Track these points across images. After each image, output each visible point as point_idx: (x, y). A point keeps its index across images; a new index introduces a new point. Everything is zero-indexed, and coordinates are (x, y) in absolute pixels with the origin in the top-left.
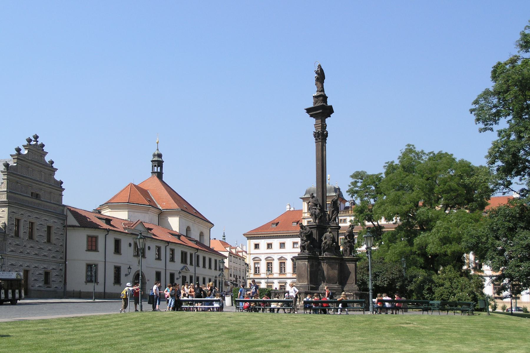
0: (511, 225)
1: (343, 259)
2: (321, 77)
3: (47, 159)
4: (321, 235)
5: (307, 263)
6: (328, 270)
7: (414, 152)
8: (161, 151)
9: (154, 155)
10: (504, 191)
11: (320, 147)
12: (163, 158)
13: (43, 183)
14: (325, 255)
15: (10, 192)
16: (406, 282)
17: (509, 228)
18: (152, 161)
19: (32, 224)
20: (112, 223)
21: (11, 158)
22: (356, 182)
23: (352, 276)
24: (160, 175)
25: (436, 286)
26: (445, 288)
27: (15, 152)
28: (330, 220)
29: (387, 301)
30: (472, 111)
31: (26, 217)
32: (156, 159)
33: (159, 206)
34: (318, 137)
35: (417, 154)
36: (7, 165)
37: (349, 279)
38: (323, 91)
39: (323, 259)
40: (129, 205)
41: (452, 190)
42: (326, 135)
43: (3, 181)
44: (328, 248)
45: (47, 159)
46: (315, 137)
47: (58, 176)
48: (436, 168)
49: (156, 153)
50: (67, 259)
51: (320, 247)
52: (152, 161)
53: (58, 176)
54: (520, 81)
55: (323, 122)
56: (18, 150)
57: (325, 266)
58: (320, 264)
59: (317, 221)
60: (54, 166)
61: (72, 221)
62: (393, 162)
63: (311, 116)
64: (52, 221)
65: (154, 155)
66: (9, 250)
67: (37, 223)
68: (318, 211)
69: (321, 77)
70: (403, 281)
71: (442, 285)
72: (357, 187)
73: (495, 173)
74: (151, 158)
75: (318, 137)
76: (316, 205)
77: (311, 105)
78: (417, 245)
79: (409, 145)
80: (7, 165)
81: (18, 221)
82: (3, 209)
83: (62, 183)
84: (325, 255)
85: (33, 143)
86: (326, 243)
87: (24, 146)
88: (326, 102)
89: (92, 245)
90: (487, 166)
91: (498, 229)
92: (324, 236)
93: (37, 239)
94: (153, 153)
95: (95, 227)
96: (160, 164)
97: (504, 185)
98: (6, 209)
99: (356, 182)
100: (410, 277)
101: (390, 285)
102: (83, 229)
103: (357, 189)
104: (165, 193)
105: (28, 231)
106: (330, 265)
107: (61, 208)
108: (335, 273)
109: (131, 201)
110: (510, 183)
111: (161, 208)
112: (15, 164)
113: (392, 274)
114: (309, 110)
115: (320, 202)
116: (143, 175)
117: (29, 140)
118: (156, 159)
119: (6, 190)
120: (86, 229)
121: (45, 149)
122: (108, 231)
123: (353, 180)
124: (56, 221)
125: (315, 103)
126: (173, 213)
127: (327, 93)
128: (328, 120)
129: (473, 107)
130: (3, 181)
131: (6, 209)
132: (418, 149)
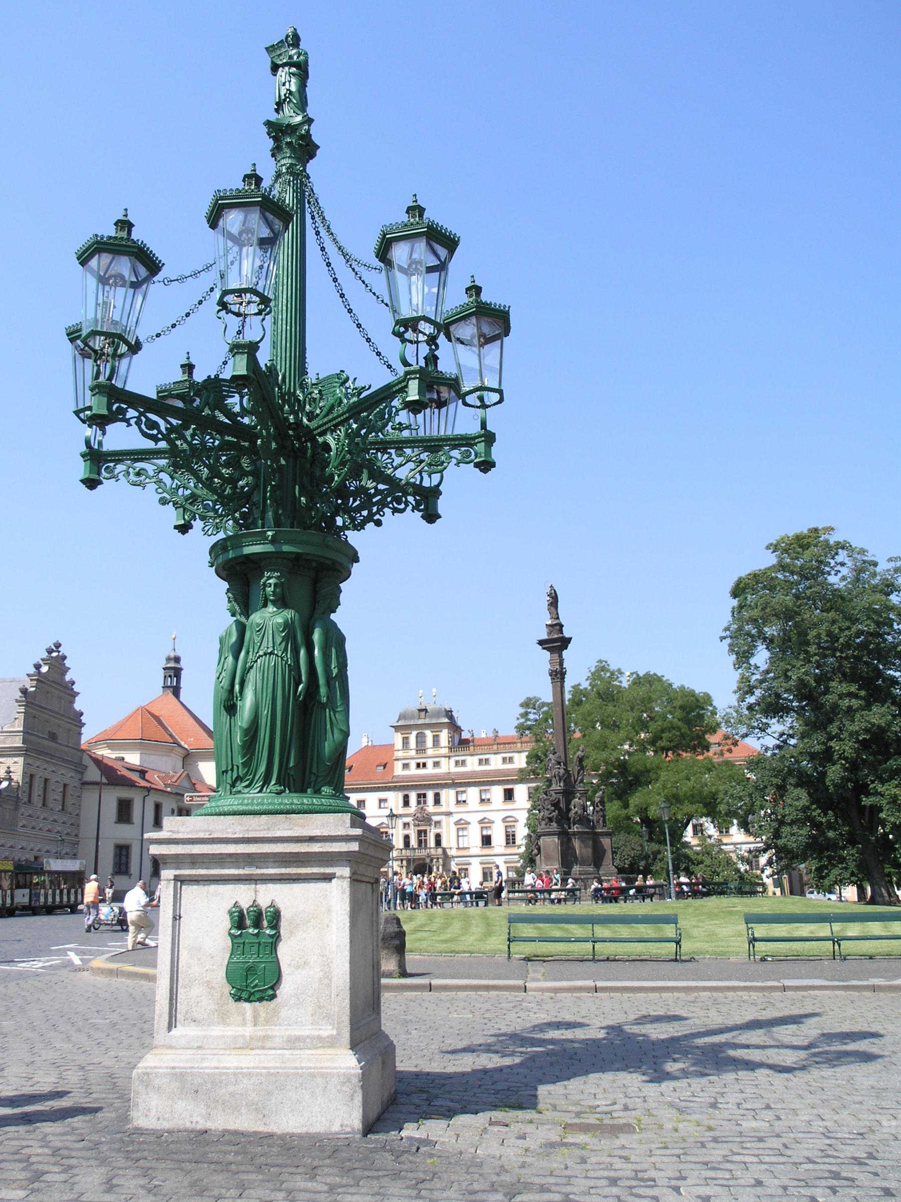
0: (780, 782)
1: (596, 833)
2: (554, 601)
3: (68, 678)
4: (568, 803)
5: (556, 840)
6: (580, 847)
7: (608, 670)
8: (179, 653)
9: (169, 659)
10: (759, 735)
11: (559, 689)
12: (183, 664)
13: (63, 715)
14: (575, 828)
15: (28, 733)
16: (650, 861)
17: (777, 785)
18: (164, 669)
19: (46, 780)
20: (147, 776)
21: (28, 679)
22: (527, 713)
23: (609, 855)
24: (176, 691)
25: (694, 864)
26: (706, 866)
27: (32, 670)
28: (575, 782)
29: (686, 884)
30: (722, 638)
31: (44, 769)
32: (172, 665)
33: (183, 743)
34: (556, 675)
35: (612, 674)
36: (24, 691)
37: (605, 860)
38: (558, 618)
39: (574, 834)
40: (143, 744)
41: (673, 728)
42: (565, 673)
43: (17, 716)
44: (578, 820)
45: (68, 678)
46: (551, 675)
47: (77, 706)
48: (650, 698)
49: (172, 655)
50: (100, 836)
51: (569, 819)
52: (164, 669)
53: (77, 706)
54: (784, 613)
55: (561, 656)
56: (38, 667)
57: (576, 844)
58: (569, 840)
59: (562, 784)
60: (76, 688)
61: (94, 774)
62: (579, 685)
63: (544, 648)
64: (68, 776)
65: (169, 659)
66: (21, 824)
67: (53, 779)
68: (562, 771)
69: (554, 601)
70: (647, 860)
71: (702, 862)
72: (529, 720)
73: (747, 712)
74: (163, 664)
75: (556, 675)
76: (559, 763)
77: (545, 636)
78: (635, 806)
79: (600, 661)
80: (24, 691)
81: (32, 776)
82: (16, 759)
83: (82, 714)
84: (575, 828)
85: (54, 654)
86: (576, 813)
87: (43, 660)
88: (561, 631)
89: (124, 812)
90: (737, 704)
91: (766, 787)
92: (573, 803)
93: (51, 806)
94: (166, 655)
95: (131, 784)
96: (176, 673)
97: (760, 729)
98: (21, 760)
99: (527, 713)
100: (652, 853)
101: (631, 865)
102: (113, 787)
103: (529, 723)
104: (192, 721)
105: (41, 793)
106: (583, 841)
107: (79, 753)
108: (588, 852)
109: (146, 736)
110: (768, 725)
111: (186, 746)
112: (33, 689)
113: (633, 849)
114: (541, 643)
115: (563, 758)
116: (151, 688)
117: (50, 651)
118: (172, 664)
119: (21, 729)
120: (117, 787)
121: (67, 663)
122: (149, 790)
123: (522, 710)
124: (73, 775)
125: (549, 633)
126: (205, 755)
127: (562, 620)
128: (565, 652)
129: (724, 634)
130: (17, 716)
131: (21, 760)
132: (613, 667)
